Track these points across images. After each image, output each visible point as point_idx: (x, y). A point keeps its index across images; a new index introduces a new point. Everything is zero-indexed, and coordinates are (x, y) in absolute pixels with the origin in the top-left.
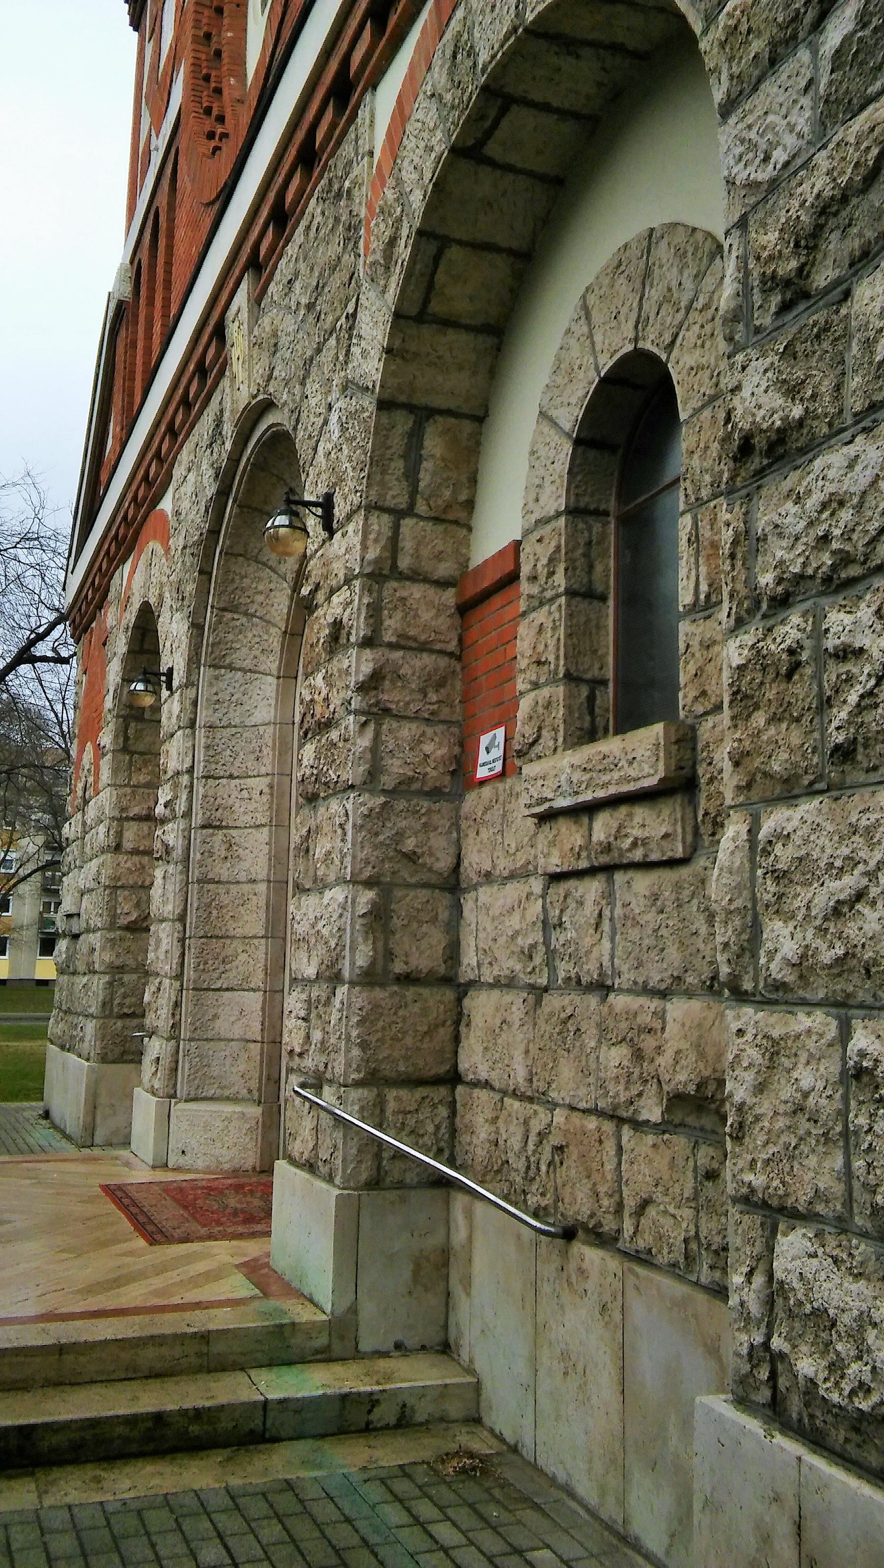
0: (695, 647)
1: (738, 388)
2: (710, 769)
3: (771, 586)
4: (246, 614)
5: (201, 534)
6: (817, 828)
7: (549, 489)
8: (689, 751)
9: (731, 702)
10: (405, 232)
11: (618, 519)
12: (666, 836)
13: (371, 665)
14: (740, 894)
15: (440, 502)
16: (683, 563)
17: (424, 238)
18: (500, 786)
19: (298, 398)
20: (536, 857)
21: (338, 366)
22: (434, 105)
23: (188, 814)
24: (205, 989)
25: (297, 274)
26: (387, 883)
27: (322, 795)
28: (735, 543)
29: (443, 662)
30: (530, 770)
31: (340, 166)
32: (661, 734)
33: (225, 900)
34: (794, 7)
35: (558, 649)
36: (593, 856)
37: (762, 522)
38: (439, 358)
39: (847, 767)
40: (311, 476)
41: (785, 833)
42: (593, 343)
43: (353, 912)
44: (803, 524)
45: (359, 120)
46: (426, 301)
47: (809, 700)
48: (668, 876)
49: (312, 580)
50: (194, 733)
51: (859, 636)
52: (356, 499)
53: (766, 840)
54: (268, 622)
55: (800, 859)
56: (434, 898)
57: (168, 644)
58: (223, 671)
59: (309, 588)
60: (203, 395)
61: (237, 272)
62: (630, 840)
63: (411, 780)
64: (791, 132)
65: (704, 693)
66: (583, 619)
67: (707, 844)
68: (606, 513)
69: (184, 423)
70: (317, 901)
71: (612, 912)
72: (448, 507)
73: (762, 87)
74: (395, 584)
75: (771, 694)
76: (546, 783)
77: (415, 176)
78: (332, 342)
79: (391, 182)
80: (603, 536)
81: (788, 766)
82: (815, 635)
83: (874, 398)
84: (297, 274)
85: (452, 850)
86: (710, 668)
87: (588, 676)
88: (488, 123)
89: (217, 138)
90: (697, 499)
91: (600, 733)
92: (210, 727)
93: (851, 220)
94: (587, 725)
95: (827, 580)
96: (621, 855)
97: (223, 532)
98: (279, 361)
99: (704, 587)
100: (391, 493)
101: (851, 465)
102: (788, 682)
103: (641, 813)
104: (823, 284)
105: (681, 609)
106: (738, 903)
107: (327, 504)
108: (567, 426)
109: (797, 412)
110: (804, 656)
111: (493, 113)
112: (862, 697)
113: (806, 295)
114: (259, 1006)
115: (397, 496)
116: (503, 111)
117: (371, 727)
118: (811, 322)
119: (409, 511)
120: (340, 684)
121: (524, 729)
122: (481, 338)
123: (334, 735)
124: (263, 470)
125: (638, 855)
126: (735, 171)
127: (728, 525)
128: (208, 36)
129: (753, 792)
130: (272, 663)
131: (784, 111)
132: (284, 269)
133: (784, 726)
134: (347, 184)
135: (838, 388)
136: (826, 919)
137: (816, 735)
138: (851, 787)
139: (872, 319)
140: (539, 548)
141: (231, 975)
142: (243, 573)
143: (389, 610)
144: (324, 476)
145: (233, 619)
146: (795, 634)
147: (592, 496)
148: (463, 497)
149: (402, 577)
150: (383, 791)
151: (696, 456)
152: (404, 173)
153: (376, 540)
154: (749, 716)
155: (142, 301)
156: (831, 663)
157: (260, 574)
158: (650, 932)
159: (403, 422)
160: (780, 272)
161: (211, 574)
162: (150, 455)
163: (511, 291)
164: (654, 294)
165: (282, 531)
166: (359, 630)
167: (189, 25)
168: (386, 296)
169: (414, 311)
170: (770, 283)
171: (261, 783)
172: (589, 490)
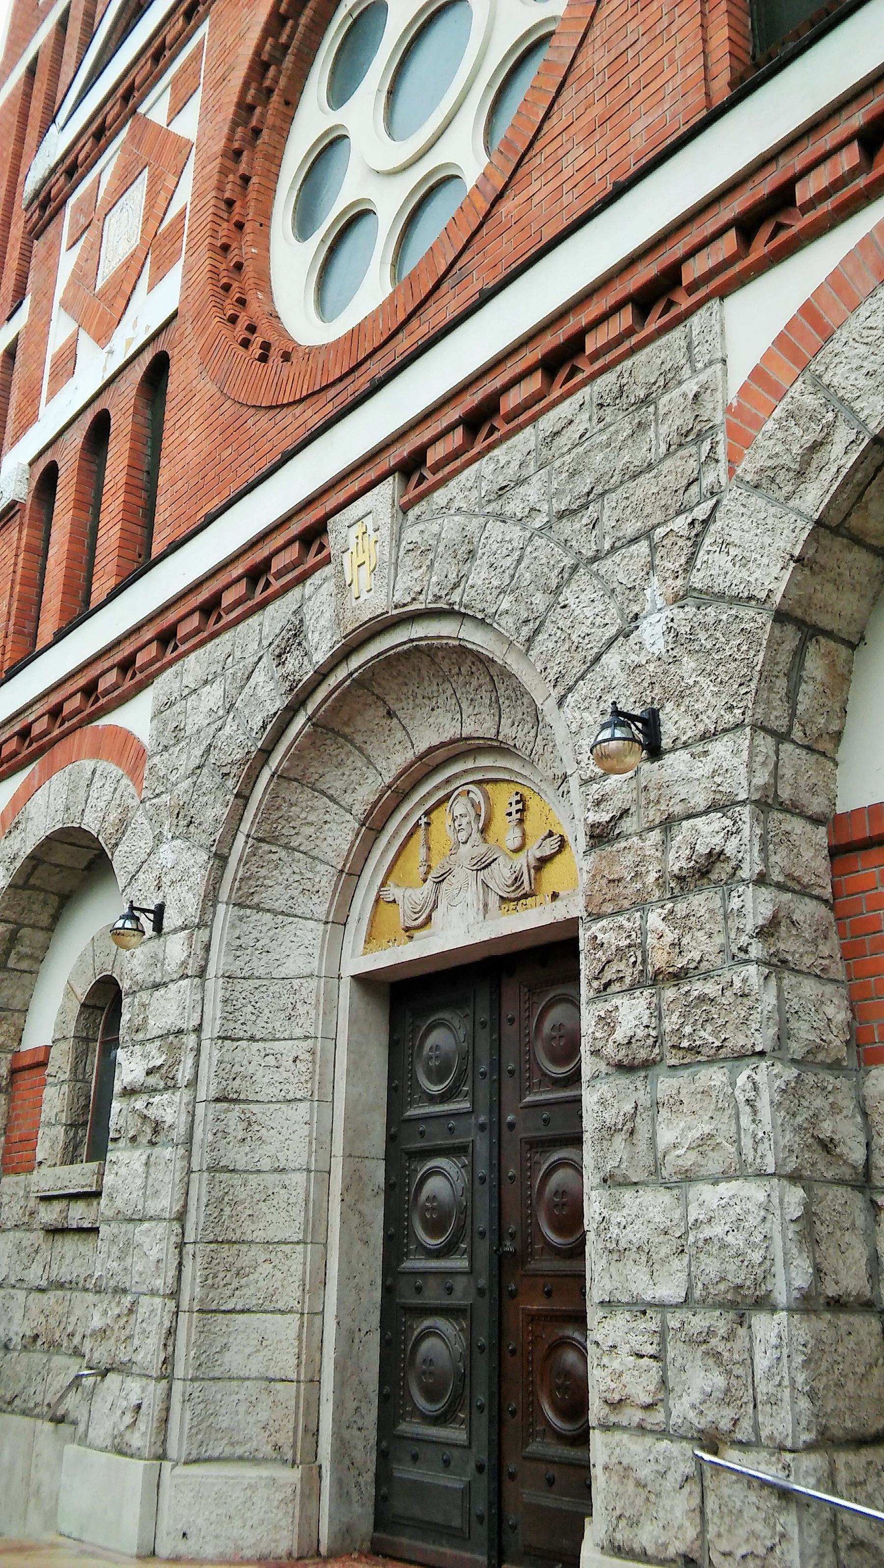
4: (286, 847)
17: (877, 447)
23: (193, 1083)
24: (229, 1312)
54: (314, 858)
58: (248, 911)
61: (371, 474)
92: (229, 977)
100: (775, 713)
114: (293, 1333)
117: (773, 981)
141: (248, 1292)
142: (293, 800)
145: (271, 852)
148: (834, 727)
149: (783, 808)
150: (793, 1061)
153: (764, 764)
157: (316, 803)
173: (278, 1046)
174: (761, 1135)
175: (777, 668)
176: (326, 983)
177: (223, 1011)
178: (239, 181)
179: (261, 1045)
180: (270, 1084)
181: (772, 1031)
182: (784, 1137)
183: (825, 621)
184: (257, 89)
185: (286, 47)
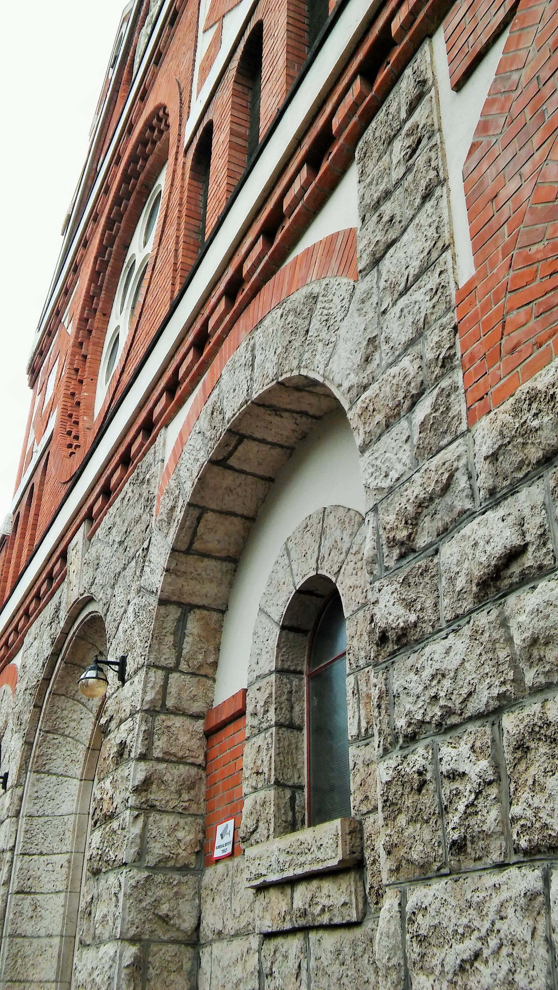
0: (360, 766)
1: (376, 602)
2: (373, 852)
3: (404, 728)
4: (63, 735)
5: (38, 681)
6: (445, 902)
7: (265, 656)
8: (358, 840)
9: (383, 807)
10: (180, 504)
11: (309, 676)
12: (345, 904)
13: (144, 774)
14: (395, 954)
15: (195, 663)
16: (349, 707)
18: (230, 863)
19: (109, 596)
20: (254, 920)
21: (136, 578)
22: (200, 437)
25: (114, 524)
26: (147, 940)
27: (104, 870)
28: (380, 698)
29: (193, 771)
30: (251, 852)
31: (144, 466)
32: (339, 828)
33: (28, 950)
34: (397, 399)
35: (270, 764)
36: (294, 919)
37: (396, 687)
38: (199, 575)
39: (461, 858)
40: (113, 645)
41: (424, 906)
42: (291, 570)
43: (120, 964)
44: (421, 688)
45: (156, 443)
46: (192, 543)
47: (433, 807)
48: (348, 935)
49: (108, 714)
50: (18, 822)
51: (462, 764)
52: (141, 660)
53: (411, 911)
54: (77, 741)
55: (435, 927)
56: (180, 952)
57: (7, 756)
58: (43, 775)
59: (106, 719)
60: (49, 593)
61: (78, 521)
62: (319, 907)
63: (168, 858)
64: (399, 462)
65: (367, 797)
66: (287, 743)
67: (373, 911)
68: (301, 673)
69: (35, 609)
70: (94, 954)
71: (308, 964)
72: (201, 666)
73: (382, 438)
74: (163, 717)
75: (408, 803)
76: (261, 862)
77: (188, 474)
78: (133, 564)
79: (173, 476)
80: (300, 687)
81: (423, 855)
82: (434, 761)
83: (458, 612)
84: (114, 524)
85: (195, 913)
86: (370, 780)
87: (290, 783)
88: (231, 448)
89: (73, 447)
90: (357, 666)
91: (299, 825)
92: (30, 816)
93: (436, 511)
94: (290, 819)
95: (439, 725)
96: (314, 920)
97: (52, 680)
98: (99, 574)
99: (364, 724)
100: (164, 657)
101: (447, 652)
102: (419, 794)
103: (327, 886)
104: (423, 545)
105: (350, 738)
106: (394, 961)
107: (122, 663)
108: (277, 618)
109: (413, 618)
110: (428, 776)
111: (233, 443)
112: (467, 806)
113: (414, 551)
115: (168, 658)
116: (240, 442)
117: (141, 819)
118: (417, 566)
119: (176, 669)
120: (122, 787)
121: (247, 822)
122: (224, 564)
123: (115, 824)
124: (83, 639)
125: (325, 919)
126: (369, 481)
127: (376, 686)
128: (73, 394)
129: (401, 874)
130: (77, 770)
131: (395, 451)
132: (107, 521)
133: (418, 825)
134: (148, 476)
135: (436, 605)
136: (455, 974)
137: (440, 833)
138: (465, 872)
139: (452, 566)
140: (258, 694)
142: (63, 707)
143: (159, 734)
144: (121, 645)
146: (421, 762)
147: (292, 661)
148: (211, 659)
149: (169, 712)
151: (355, 640)
152: (181, 472)
153: (153, 687)
154: (395, 818)
155: (18, 536)
156: (446, 781)
157: (76, 708)
158: (335, 981)
159: (174, 613)
160: (398, 537)
161: (41, 707)
162: (10, 629)
163: (243, 538)
164: (327, 544)
165: (91, 681)
166: (137, 748)
167: (62, 388)
168: (167, 539)
169: (184, 547)
170: (393, 542)
171: (62, 859)
172: (290, 658)
173: (54, 858)
174: (117, 914)
175: (164, 631)
176: (80, 818)
177: (24, 837)
178: (81, 358)
179: (45, 857)
180: (49, 882)
181: (134, 850)
182: (129, 915)
183: (196, 600)
184: (88, 310)
185: (101, 287)
